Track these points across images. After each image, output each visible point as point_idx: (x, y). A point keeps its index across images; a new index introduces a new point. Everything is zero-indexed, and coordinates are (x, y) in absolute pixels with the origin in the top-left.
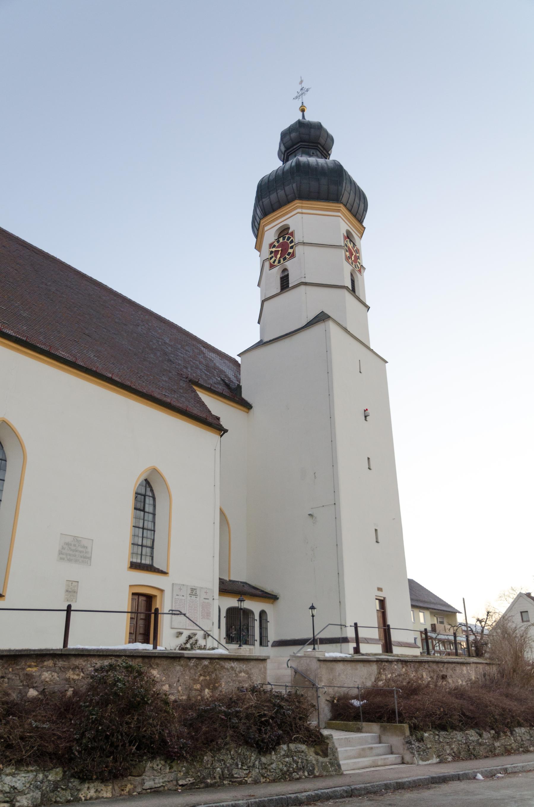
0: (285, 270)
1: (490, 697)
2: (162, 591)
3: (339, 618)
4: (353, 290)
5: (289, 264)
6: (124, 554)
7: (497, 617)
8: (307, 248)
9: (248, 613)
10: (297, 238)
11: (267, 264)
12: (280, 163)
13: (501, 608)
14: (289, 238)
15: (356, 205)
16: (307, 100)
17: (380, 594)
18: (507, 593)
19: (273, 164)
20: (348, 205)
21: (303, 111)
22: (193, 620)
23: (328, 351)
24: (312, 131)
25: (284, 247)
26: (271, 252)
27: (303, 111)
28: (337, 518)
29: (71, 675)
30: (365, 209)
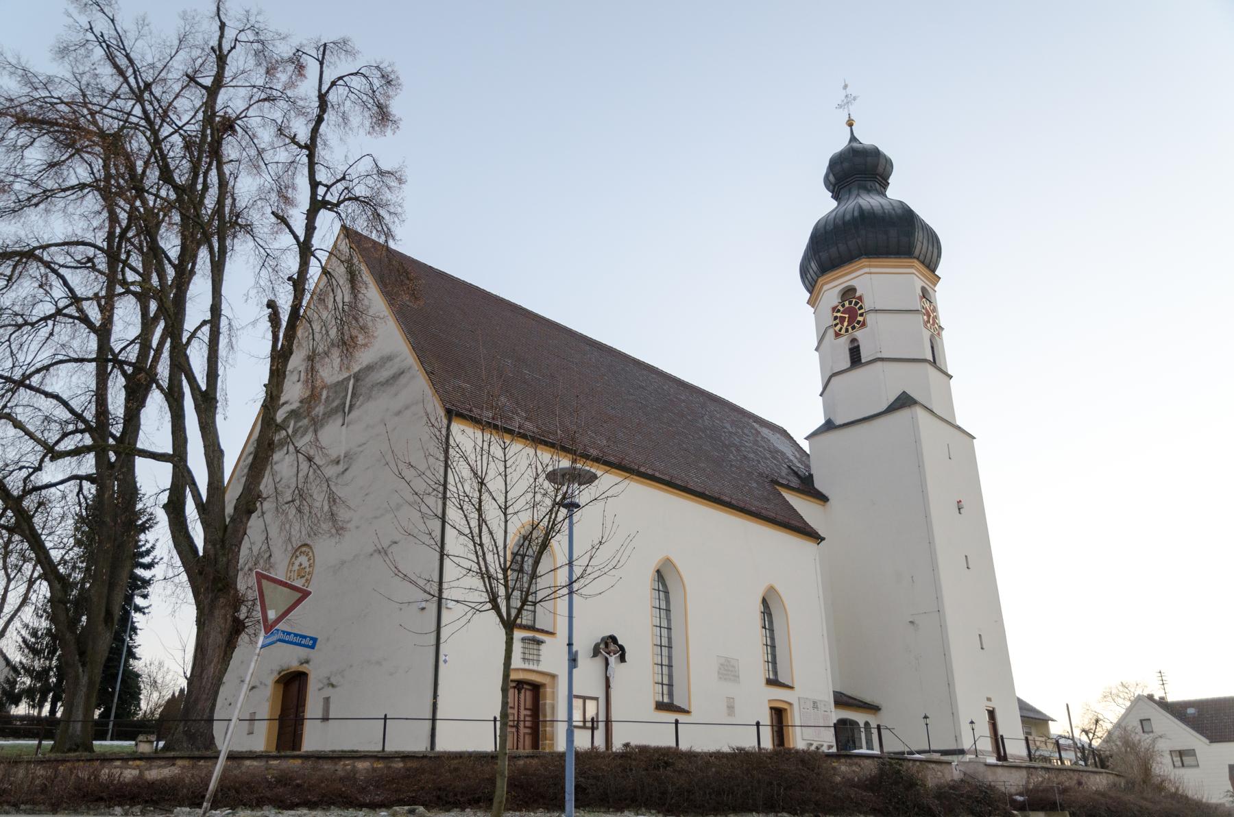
0: (854, 340)
1: (1130, 797)
2: (790, 704)
3: (949, 729)
4: (934, 363)
5: (859, 334)
6: (760, 672)
7: (1107, 726)
8: (880, 316)
9: (854, 724)
10: (867, 304)
11: (831, 333)
12: (834, 204)
13: (1112, 714)
14: (856, 303)
15: (929, 255)
16: (856, 112)
17: (989, 704)
18: (1114, 691)
19: (824, 205)
20: (922, 258)
21: (851, 125)
22: (812, 734)
23: (917, 441)
24: (869, 159)
25: (850, 312)
26: (836, 318)
27: (851, 125)
28: (942, 627)
29: (854, 768)
30: (939, 255)
